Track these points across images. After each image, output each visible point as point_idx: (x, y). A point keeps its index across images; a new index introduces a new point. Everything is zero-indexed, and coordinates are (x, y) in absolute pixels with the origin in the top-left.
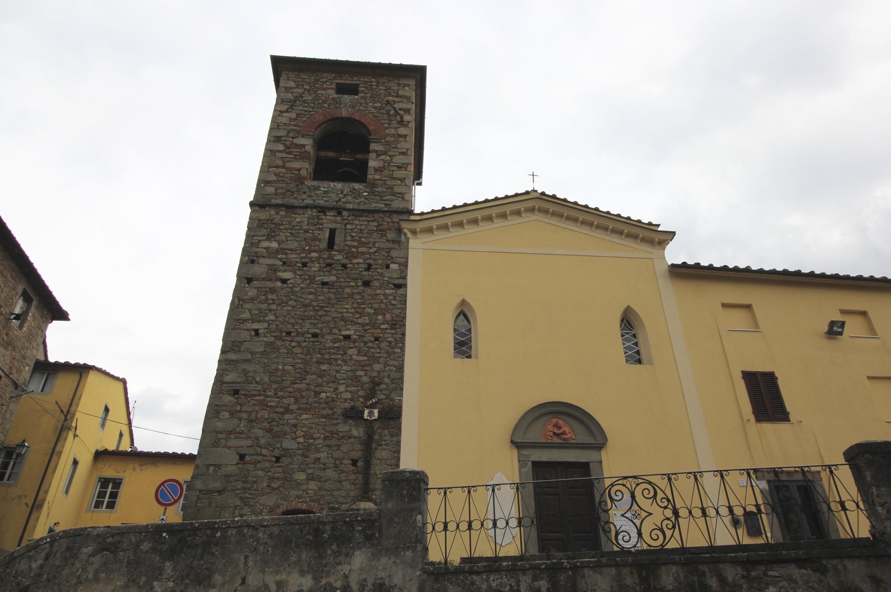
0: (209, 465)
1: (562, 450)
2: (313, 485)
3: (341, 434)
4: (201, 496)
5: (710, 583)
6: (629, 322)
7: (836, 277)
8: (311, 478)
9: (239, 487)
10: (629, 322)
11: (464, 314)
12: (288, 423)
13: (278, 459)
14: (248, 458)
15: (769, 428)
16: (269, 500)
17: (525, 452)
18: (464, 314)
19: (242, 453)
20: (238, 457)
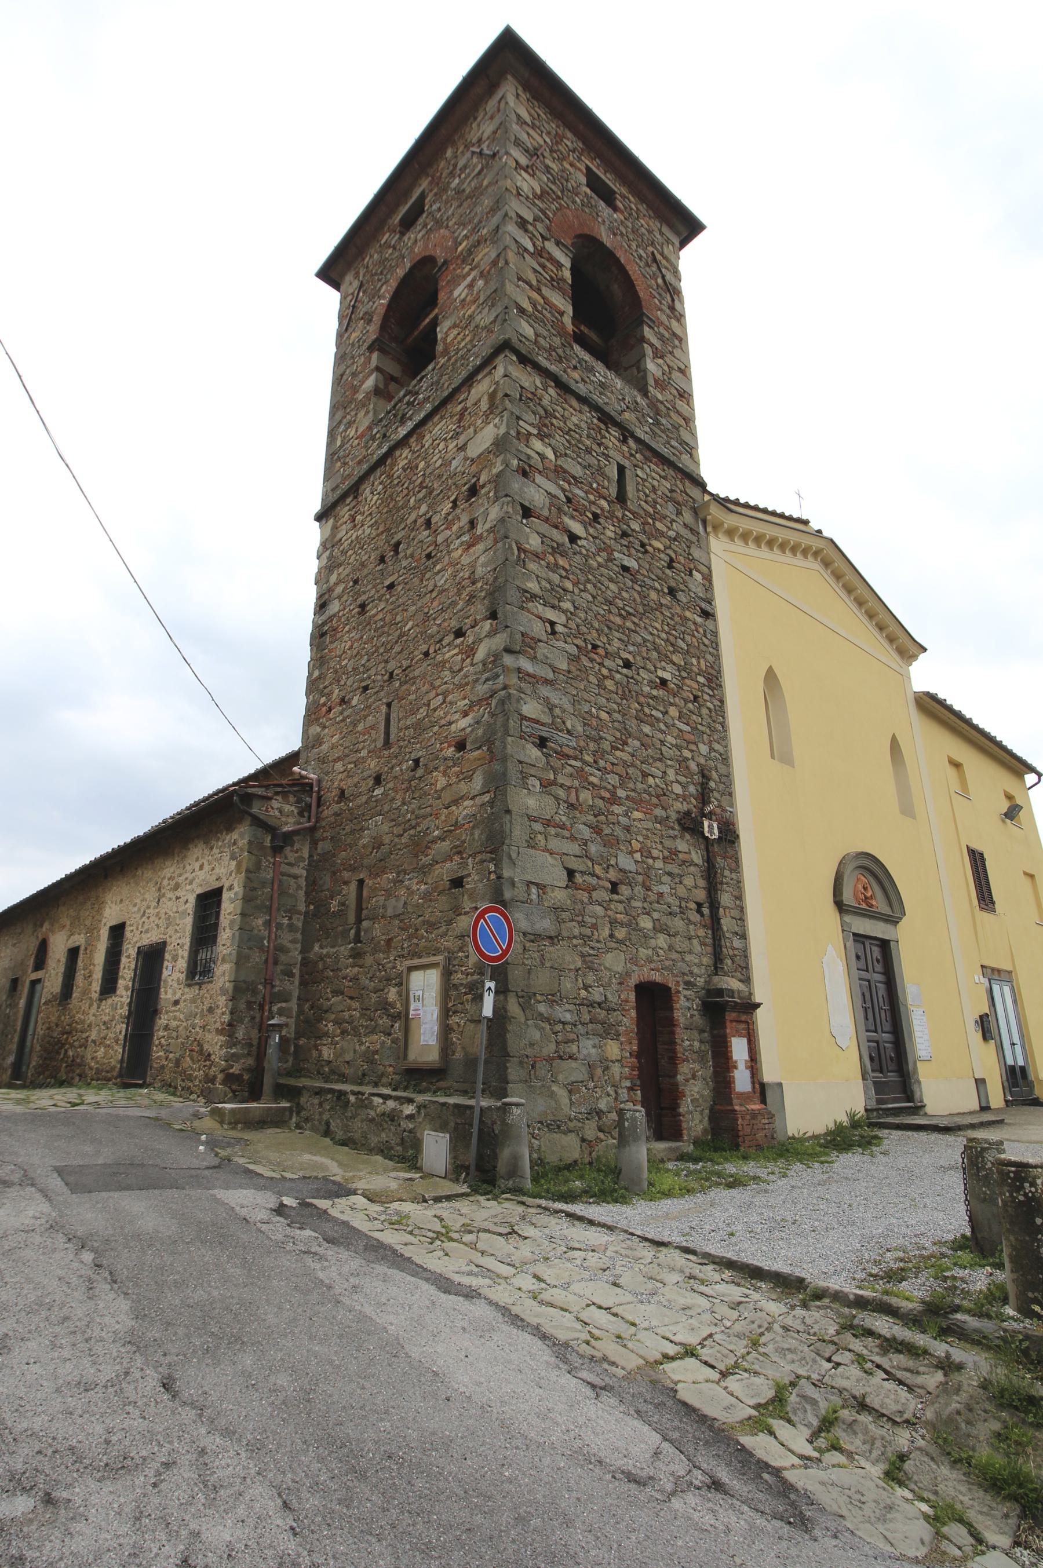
0: (529, 883)
1: (872, 921)
2: (662, 940)
3: (681, 856)
4: (528, 945)
5: (103, 1092)
6: (895, 745)
7: (958, 715)
8: (660, 928)
9: (576, 932)
10: (895, 745)
11: (770, 676)
12: (619, 823)
13: (614, 888)
14: (579, 879)
15: (985, 914)
16: (614, 961)
17: (847, 918)
18: (770, 676)
19: (570, 866)
20: (565, 873)
